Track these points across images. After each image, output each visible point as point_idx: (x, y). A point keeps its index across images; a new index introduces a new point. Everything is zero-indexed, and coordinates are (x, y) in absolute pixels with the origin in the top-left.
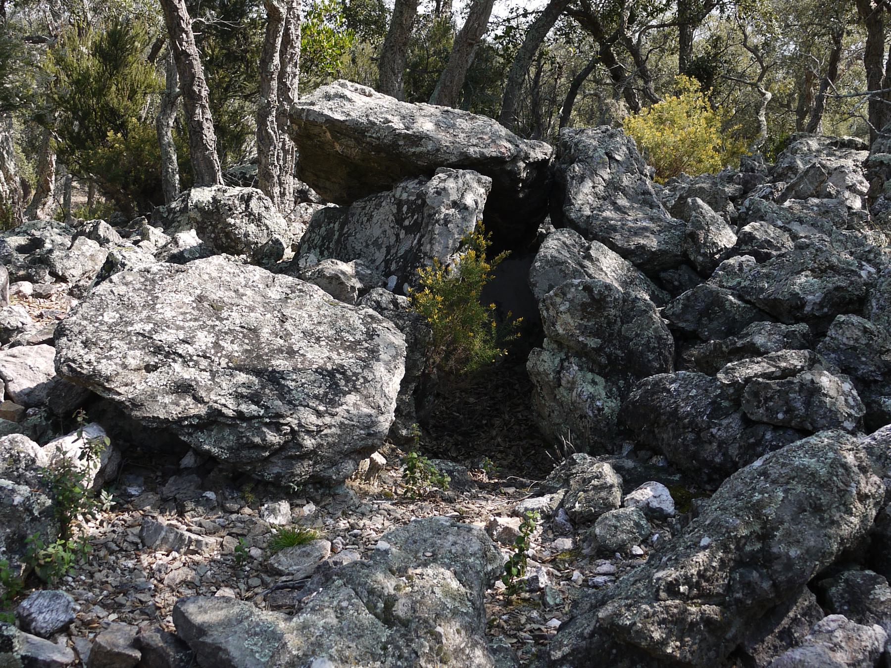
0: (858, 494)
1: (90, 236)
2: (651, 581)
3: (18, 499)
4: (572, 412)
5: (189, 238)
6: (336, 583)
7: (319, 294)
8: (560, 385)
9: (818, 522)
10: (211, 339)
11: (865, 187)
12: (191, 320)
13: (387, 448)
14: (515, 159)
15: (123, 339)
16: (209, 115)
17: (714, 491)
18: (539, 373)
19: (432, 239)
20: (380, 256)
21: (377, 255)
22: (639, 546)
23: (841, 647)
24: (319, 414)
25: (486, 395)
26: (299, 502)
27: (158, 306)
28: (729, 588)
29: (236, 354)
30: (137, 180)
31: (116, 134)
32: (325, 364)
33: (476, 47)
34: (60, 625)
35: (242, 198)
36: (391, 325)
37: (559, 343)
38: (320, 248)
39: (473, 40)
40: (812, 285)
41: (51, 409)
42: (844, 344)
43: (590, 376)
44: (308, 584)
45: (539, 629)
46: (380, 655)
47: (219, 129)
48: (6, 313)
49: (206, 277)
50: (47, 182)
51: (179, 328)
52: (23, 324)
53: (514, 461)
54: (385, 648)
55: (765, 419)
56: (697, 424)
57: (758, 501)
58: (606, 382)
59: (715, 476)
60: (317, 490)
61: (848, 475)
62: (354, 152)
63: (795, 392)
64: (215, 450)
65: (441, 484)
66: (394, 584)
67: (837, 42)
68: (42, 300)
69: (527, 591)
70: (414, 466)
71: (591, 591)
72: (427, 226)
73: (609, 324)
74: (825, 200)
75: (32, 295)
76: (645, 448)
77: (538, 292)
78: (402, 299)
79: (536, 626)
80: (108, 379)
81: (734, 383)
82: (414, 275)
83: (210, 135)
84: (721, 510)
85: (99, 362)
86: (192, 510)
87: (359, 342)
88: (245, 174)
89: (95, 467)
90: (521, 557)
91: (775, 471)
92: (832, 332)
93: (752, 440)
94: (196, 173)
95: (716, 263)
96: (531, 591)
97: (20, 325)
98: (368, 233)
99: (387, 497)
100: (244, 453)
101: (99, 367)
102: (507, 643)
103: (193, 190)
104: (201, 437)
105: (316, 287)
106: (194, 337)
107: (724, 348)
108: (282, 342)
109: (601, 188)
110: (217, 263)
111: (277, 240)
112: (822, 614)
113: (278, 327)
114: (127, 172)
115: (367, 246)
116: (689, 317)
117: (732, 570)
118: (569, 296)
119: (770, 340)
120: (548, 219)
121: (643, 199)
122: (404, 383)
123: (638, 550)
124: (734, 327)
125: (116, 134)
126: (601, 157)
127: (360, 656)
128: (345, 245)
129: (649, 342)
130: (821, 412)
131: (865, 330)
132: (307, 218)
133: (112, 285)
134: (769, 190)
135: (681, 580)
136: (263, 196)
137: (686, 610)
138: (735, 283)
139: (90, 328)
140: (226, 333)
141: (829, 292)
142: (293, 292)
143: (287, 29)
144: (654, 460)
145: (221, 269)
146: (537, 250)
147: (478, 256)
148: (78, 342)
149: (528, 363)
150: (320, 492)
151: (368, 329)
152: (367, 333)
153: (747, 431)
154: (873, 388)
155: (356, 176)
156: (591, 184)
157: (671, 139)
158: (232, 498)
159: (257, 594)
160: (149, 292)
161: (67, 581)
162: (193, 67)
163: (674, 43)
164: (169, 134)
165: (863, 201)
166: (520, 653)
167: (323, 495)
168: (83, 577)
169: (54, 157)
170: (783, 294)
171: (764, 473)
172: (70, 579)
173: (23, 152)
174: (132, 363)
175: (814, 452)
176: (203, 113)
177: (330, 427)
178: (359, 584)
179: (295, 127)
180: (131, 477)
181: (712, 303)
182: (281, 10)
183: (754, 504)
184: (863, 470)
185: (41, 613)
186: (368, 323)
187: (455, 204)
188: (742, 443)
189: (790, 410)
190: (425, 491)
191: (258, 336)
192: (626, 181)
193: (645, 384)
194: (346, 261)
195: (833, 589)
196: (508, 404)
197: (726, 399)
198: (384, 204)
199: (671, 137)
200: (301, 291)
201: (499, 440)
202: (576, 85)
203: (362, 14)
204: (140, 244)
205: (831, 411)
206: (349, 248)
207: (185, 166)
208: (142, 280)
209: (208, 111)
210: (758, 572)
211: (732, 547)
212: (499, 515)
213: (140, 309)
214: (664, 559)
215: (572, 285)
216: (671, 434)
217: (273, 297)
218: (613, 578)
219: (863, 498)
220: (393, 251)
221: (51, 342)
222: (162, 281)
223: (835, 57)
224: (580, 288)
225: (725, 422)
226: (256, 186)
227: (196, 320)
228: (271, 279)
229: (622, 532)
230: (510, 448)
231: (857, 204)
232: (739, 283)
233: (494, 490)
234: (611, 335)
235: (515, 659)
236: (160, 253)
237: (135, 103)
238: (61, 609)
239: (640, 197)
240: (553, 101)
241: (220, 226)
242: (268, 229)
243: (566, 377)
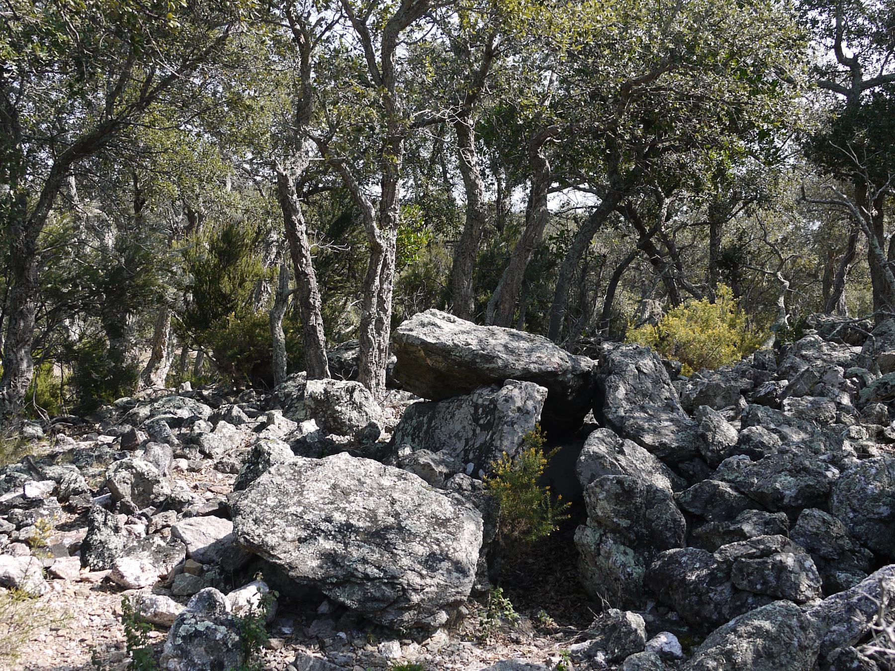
1: (224, 418)
3: (219, 636)
4: (608, 575)
8: (599, 554)
9: (771, 665)
15: (282, 518)
16: (321, 321)
18: (583, 545)
20: (460, 446)
21: (458, 445)
24: (422, 577)
25: (541, 556)
26: (406, 641)
27: (305, 493)
35: (347, 390)
41: (222, 567)
43: (622, 548)
49: (337, 469)
62: (442, 366)
64: (348, 602)
72: (498, 425)
73: (637, 509)
77: (583, 479)
78: (477, 482)
80: (273, 548)
81: (726, 561)
82: (488, 463)
93: (738, 603)
95: (721, 458)
98: (451, 427)
100: (369, 604)
101: (266, 539)
105: (416, 476)
107: (720, 529)
115: (450, 438)
118: (606, 487)
124: (732, 512)
129: (666, 523)
130: (788, 584)
134: (773, 387)
139: (258, 509)
140: (354, 514)
141: (802, 489)
143: (385, 260)
144: (669, 615)
145: (347, 462)
150: (421, 634)
174: (290, 536)
189: (765, 583)
191: (376, 515)
206: (436, 439)
209: (320, 318)
215: (608, 479)
220: (471, 443)
225: (719, 589)
227: (332, 503)
230: (561, 600)
234: (638, 517)
243: (604, 548)
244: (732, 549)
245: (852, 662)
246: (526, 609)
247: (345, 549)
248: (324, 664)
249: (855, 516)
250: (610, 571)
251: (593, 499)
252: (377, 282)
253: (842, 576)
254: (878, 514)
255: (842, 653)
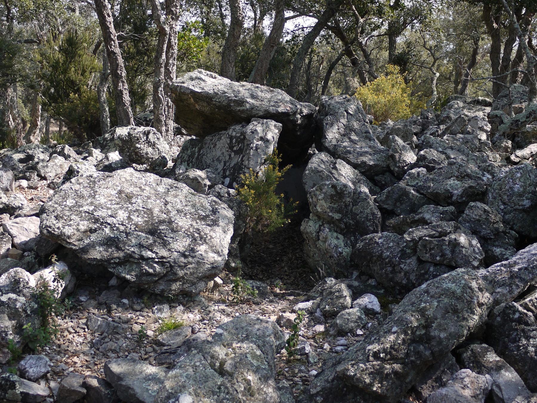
0: (478, 303)
2: (365, 351)
4: (325, 254)
5: (115, 156)
6: (193, 352)
7: (186, 189)
8: (319, 239)
9: (456, 318)
10: (126, 215)
11: (488, 128)
12: (115, 204)
13: (223, 275)
14: (295, 113)
15: (77, 215)
16: (126, 86)
17: (402, 299)
18: (307, 233)
19: (249, 158)
20: (220, 167)
22: (361, 329)
23: (468, 387)
25: (279, 243)
27: (97, 196)
28: (407, 355)
29: (140, 223)
30: (86, 121)
31: (75, 94)
32: (189, 228)
33: (275, 48)
34: (42, 374)
36: (226, 206)
37: (319, 216)
38: (187, 161)
39: (274, 44)
40: (457, 185)
41: (37, 253)
42: (474, 218)
43: (335, 234)
44: (179, 351)
45: (305, 376)
46: (217, 392)
47: (132, 93)
48: (12, 199)
49: (123, 180)
50: (36, 121)
51: (108, 209)
52: (22, 205)
53: (294, 280)
54: (219, 388)
55: (430, 260)
56: (393, 262)
57: (424, 307)
58: (344, 238)
59: (403, 291)
60: (184, 298)
61: (473, 292)
62: (207, 110)
63: (446, 245)
64: (128, 277)
65: (253, 294)
66: (225, 352)
67: (476, 44)
68: (33, 190)
69: (299, 355)
70: (238, 285)
71: (334, 355)
72: (246, 150)
74: (466, 136)
75: (27, 187)
76: (365, 274)
78: (232, 191)
79: (303, 374)
80: (69, 237)
81: (413, 240)
82: (239, 177)
83: (127, 98)
84: (404, 312)
85: (64, 228)
86: (115, 309)
87: (207, 216)
88: (147, 118)
89: (61, 286)
90: (294, 336)
91: (432, 291)
92: (467, 212)
93: (423, 272)
94: (119, 119)
95: (405, 172)
96: (301, 355)
97: (21, 205)
99: (223, 302)
100: (144, 278)
101: (64, 231)
102: (286, 384)
103: (117, 129)
104: (120, 269)
105: (185, 185)
106: (116, 213)
107: (408, 220)
108: (165, 216)
109: (342, 130)
110: (130, 172)
111: (164, 157)
112: (459, 368)
113: (163, 207)
114: (81, 116)
115: (213, 161)
116: (390, 202)
117: (409, 345)
118: (324, 191)
119: (433, 216)
120: (314, 145)
121: (367, 137)
122: (233, 239)
123: (360, 332)
124: (414, 208)
125: (75, 94)
126: (342, 113)
127: (206, 392)
128: (201, 161)
130: (460, 256)
131: (485, 211)
132: (181, 143)
133: (71, 184)
134: (435, 129)
135: (381, 351)
136: (156, 132)
137: (384, 367)
138: (415, 183)
139: (59, 208)
140: (134, 211)
141: (466, 189)
142: (172, 188)
143: (170, 39)
144: (370, 281)
145: (132, 175)
146: (306, 163)
147: (274, 168)
148: (52, 216)
149: (301, 227)
150: (186, 299)
151: (213, 208)
152: (213, 211)
153: (420, 266)
154: (489, 242)
155: (209, 123)
156: (337, 128)
157: (383, 100)
158: (138, 303)
159: (150, 356)
160: (92, 188)
161: (46, 350)
162: (117, 60)
163: (386, 44)
164: (104, 96)
165: (487, 136)
166: (294, 390)
167: (187, 301)
168: (55, 347)
169: (40, 107)
170: (441, 189)
171: (427, 292)
172: (47, 348)
173: (23, 103)
175: (454, 280)
176: (123, 85)
177: (191, 264)
178: (206, 353)
179: (174, 95)
180: (82, 291)
181: (402, 195)
182: (166, 29)
183: (421, 309)
184: (481, 290)
185: (31, 368)
186: (213, 205)
187: (262, 139)
188: (417, 273)
189: (443, 255)
190: (244, 298)
191: (152, 213)
192: (356, 125)
193: (365, 239)
194: (202, 169)
195: (465, 355)
196: (291, 248)
197: (409, 248)
198: (222, 138)
199: (382, 99)
200: (176, 187)
201: (286, 268)
202: (332, 67)
203: (212, 28)
204: (88, 159)
205: (465, 255)
206: (203, 162)
207: (113, 113)
208: (88, 181)
210: (423, 346)
211: (409, 332)
212: (284, 312)
213: (87, 198)
214: (373, 339)
215: (326, 185)
216: (379, 267)
217: (161, 191)
218: (346, 347)
219: (480, 305)
220: (227, 164)
221: (37, 215)
222: (99, 182)
223: (475, 53)
224: (330, 186)
225: (408, 261)
226: (152, 126)
227: (118, 204)
228: (159, 181)
229: (352, 322)
230: (292, 273)
231: (483, 137)
232: (417, 183)
233: (282, 297)
234: (347, 212)
235: (292, 393)
236: (99, 165)
237: (85, 77)
238: (42, 365)
239: (364, 135)
240: (318, 77)
241: (132, 149)
242: (159, 150)
243: (322, 235)
244: (419, 232)
245: (514, 313)
246: (268, 279)
247: (127, 237)
248: (109, 324)
249: (505, 208)
250: (327, 251)
251: (314, 200)
252: (164, 57)
253: (498, 251)
254: (522, 205)
255: (506, 307)
